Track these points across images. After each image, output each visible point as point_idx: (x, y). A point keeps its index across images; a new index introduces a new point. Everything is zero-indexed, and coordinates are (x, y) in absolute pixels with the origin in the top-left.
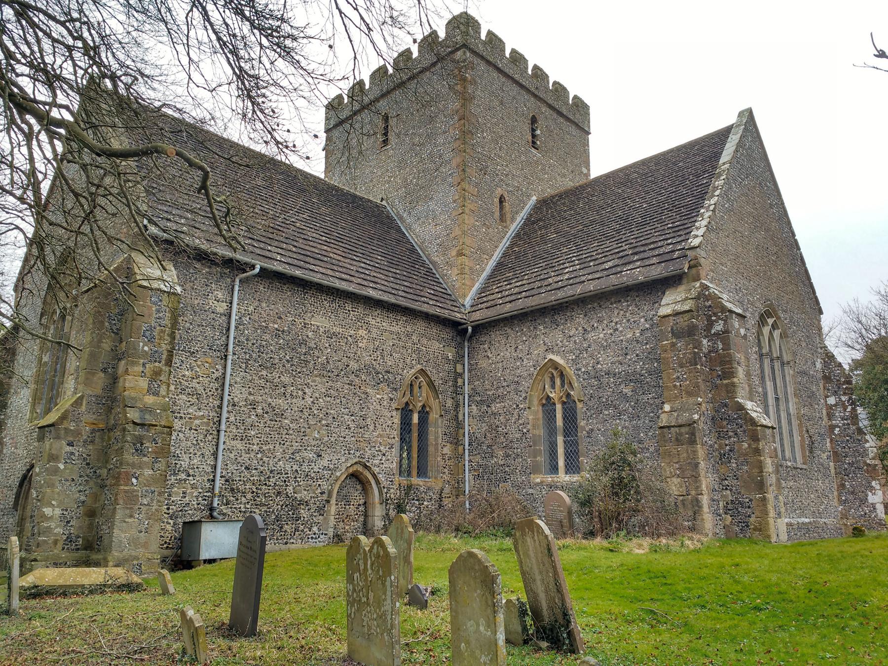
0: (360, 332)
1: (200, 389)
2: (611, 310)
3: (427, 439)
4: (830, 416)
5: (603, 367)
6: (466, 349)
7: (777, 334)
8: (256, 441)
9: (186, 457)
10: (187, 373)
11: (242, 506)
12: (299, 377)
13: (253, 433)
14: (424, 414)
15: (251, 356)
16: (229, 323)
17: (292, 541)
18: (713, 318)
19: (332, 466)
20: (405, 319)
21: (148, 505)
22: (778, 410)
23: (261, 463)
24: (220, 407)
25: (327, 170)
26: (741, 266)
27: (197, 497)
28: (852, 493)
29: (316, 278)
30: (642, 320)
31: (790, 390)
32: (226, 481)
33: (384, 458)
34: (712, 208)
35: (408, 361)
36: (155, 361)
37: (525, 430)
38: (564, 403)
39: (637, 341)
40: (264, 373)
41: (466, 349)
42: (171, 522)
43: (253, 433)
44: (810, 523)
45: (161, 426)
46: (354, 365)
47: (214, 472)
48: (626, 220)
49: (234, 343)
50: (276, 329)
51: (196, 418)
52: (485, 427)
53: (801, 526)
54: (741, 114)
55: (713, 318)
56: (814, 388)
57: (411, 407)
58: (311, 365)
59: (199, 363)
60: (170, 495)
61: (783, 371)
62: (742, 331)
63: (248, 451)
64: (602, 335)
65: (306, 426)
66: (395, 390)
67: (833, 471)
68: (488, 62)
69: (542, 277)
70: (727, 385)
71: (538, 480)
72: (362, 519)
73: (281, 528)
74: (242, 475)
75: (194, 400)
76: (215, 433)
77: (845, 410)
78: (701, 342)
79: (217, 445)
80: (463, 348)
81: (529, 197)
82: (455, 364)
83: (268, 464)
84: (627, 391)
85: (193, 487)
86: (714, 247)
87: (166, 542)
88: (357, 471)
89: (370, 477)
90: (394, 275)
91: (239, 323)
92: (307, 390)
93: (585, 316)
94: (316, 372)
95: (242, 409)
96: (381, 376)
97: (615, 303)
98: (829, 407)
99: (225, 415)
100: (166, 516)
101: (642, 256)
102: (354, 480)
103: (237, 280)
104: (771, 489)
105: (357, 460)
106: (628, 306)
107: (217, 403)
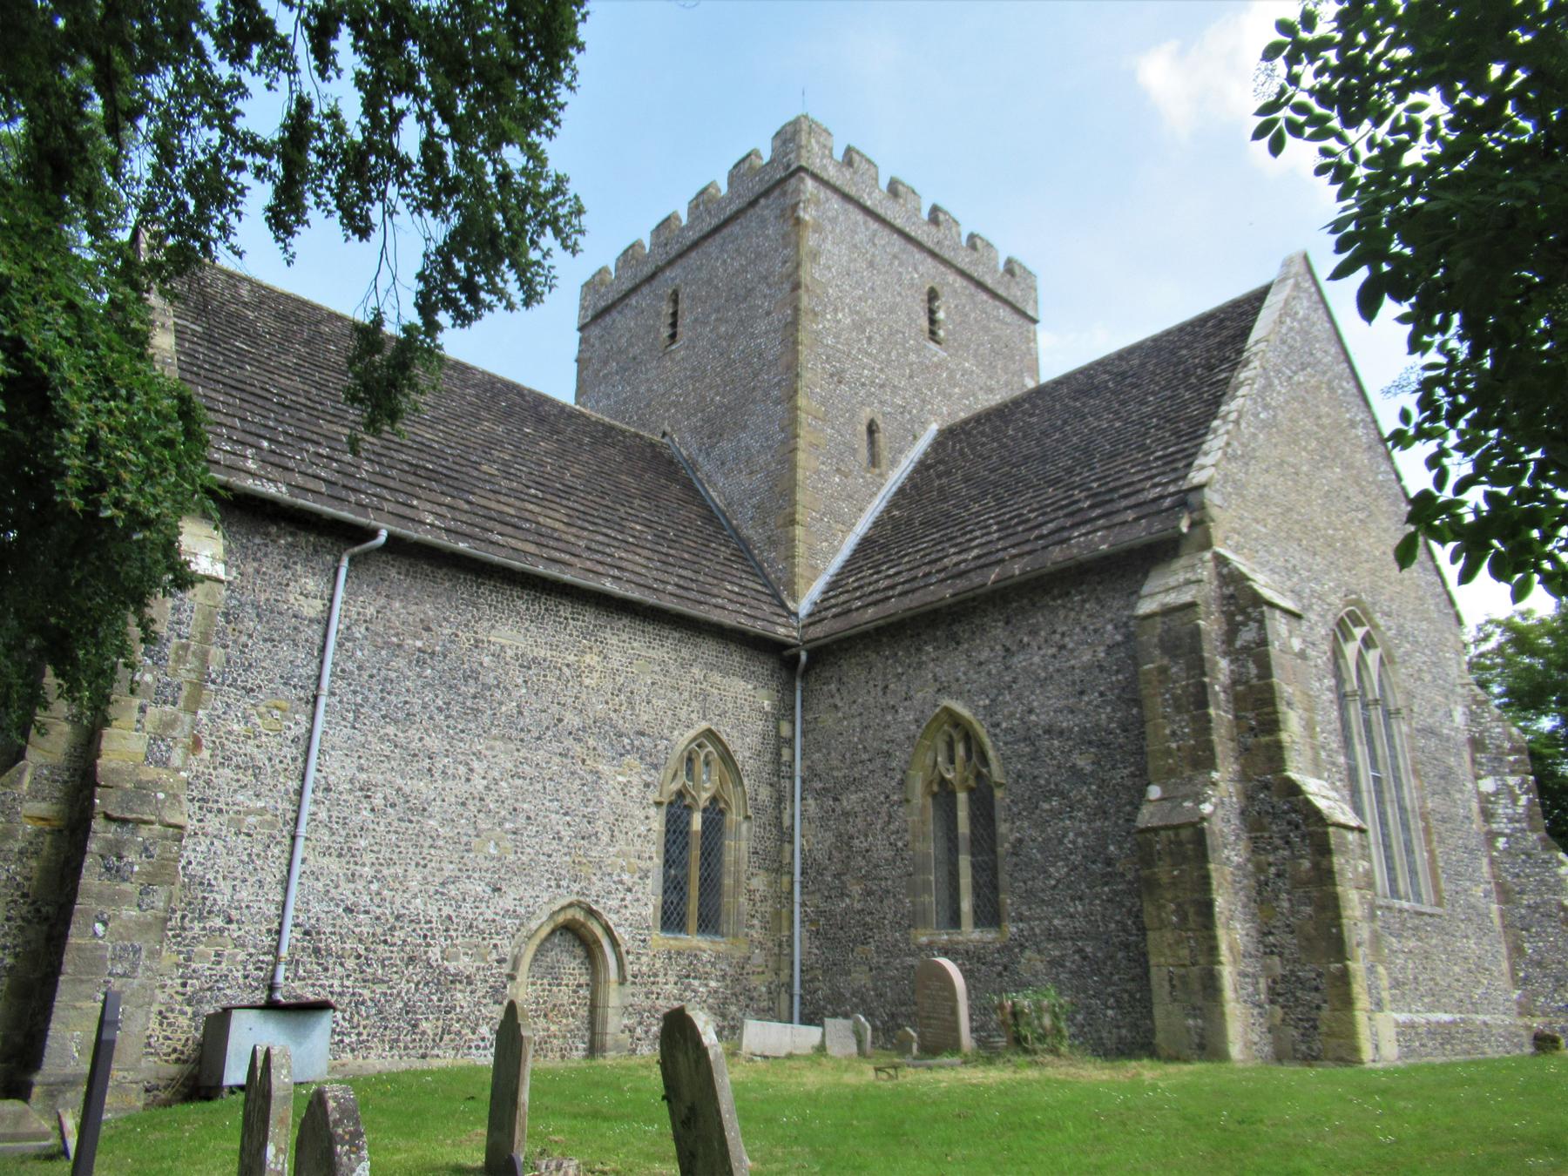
0: (587, 658)
1: (261, 758)
2: (1054, 610)
3: (719, 861)
4: (1487, 815)
5: (1039, 719)
6: (798, 694)
7: (1372, 657)
8: (369, 858)
9: (225, 886)
10: (236, 727)
11: (336, 983)
12: (461, 740)
13: (363, 843)
14: (715, 815)
15: (366, 699)
16: (325, 636)
17: (436, 1051)
18: (1239, 618)
19: (521, 910)
20: (677, 635)
21: (124, 975)
22: (1380, 801)
23: (377, 900)
24: (300, 793)
25: (581, 391)
26: (1296, 527)
27: (244, 964)
28: (1539, 964)
29: (497, 558)
30: (1110, 627)
31: (1404, 763)
32: (307, 933)
33: (629, 897)
34: (1233, 416)
35: (683, 714)
36: (165, 702)
37: (900, 844)
38: (971, 791)
39: (1101, 668)
40: (391, 730)
41: (798, 694)
42: (189, 1010)
43: (363, 843)
44: (1453, 1023)
45: (162, 823)
46: (572, 720)
47: (282, 916)
48: (1085, 451)
49: (333, 674)
50: (420, 650)
51: (248, 813)
52: (830, 838)
53: (1434, 1030)
54: (1287, 263)
55: (1239, 618)
56: (1452, 761)
57: (688, 801)
58: (486, 719)
59: (262, 709)
60: (189, 959)
61: (1388, 726)
62: (1296, 644)
63: (352, 878)
64: (1036, 659)
65: (472, 832)
66: (656, 767)
67: (1497, 921)
68: (847, 197)
69: (933, 556)
70: (1268, 746)
71: (924, 940)
72: (584, 1012)
73: (415, 1026)
74: (339, 922)
75: (247, 779)
76: (287, 841)
77: (1515, 800)
78: (1216, 663)
79: (290, 864)
80: (793, 692)
81: (924, 425)
82: (778, 720)
83: (392, 903)
84: (1083, 762)
85: (239, 943)
86: (1239, 487)
87: (175, 1050)
88: (574, 920)
89: (599, 931)
90: (663, 558)
91: (346, 637)
92: (475, 765)
93: (1007, 623)
94: (494, 731)
95: (345, 797)
96: (626, 741)
97: (1060, 596)
98: (1484, 799)
99: (308, 808)
100: (179, 998)
101: (1109, 508)
102: (569, 936)
103: (345, 563)
104: (1360, 952)
105: (574, 898)
106: (1084, 601)
107: (295, 784)
